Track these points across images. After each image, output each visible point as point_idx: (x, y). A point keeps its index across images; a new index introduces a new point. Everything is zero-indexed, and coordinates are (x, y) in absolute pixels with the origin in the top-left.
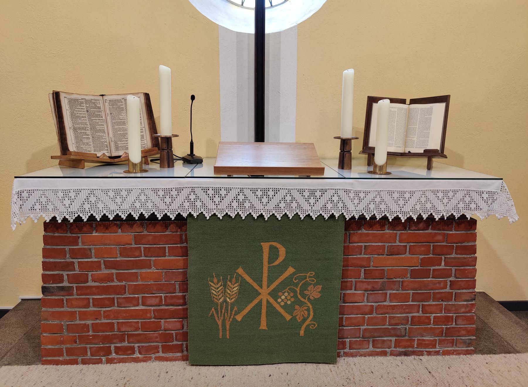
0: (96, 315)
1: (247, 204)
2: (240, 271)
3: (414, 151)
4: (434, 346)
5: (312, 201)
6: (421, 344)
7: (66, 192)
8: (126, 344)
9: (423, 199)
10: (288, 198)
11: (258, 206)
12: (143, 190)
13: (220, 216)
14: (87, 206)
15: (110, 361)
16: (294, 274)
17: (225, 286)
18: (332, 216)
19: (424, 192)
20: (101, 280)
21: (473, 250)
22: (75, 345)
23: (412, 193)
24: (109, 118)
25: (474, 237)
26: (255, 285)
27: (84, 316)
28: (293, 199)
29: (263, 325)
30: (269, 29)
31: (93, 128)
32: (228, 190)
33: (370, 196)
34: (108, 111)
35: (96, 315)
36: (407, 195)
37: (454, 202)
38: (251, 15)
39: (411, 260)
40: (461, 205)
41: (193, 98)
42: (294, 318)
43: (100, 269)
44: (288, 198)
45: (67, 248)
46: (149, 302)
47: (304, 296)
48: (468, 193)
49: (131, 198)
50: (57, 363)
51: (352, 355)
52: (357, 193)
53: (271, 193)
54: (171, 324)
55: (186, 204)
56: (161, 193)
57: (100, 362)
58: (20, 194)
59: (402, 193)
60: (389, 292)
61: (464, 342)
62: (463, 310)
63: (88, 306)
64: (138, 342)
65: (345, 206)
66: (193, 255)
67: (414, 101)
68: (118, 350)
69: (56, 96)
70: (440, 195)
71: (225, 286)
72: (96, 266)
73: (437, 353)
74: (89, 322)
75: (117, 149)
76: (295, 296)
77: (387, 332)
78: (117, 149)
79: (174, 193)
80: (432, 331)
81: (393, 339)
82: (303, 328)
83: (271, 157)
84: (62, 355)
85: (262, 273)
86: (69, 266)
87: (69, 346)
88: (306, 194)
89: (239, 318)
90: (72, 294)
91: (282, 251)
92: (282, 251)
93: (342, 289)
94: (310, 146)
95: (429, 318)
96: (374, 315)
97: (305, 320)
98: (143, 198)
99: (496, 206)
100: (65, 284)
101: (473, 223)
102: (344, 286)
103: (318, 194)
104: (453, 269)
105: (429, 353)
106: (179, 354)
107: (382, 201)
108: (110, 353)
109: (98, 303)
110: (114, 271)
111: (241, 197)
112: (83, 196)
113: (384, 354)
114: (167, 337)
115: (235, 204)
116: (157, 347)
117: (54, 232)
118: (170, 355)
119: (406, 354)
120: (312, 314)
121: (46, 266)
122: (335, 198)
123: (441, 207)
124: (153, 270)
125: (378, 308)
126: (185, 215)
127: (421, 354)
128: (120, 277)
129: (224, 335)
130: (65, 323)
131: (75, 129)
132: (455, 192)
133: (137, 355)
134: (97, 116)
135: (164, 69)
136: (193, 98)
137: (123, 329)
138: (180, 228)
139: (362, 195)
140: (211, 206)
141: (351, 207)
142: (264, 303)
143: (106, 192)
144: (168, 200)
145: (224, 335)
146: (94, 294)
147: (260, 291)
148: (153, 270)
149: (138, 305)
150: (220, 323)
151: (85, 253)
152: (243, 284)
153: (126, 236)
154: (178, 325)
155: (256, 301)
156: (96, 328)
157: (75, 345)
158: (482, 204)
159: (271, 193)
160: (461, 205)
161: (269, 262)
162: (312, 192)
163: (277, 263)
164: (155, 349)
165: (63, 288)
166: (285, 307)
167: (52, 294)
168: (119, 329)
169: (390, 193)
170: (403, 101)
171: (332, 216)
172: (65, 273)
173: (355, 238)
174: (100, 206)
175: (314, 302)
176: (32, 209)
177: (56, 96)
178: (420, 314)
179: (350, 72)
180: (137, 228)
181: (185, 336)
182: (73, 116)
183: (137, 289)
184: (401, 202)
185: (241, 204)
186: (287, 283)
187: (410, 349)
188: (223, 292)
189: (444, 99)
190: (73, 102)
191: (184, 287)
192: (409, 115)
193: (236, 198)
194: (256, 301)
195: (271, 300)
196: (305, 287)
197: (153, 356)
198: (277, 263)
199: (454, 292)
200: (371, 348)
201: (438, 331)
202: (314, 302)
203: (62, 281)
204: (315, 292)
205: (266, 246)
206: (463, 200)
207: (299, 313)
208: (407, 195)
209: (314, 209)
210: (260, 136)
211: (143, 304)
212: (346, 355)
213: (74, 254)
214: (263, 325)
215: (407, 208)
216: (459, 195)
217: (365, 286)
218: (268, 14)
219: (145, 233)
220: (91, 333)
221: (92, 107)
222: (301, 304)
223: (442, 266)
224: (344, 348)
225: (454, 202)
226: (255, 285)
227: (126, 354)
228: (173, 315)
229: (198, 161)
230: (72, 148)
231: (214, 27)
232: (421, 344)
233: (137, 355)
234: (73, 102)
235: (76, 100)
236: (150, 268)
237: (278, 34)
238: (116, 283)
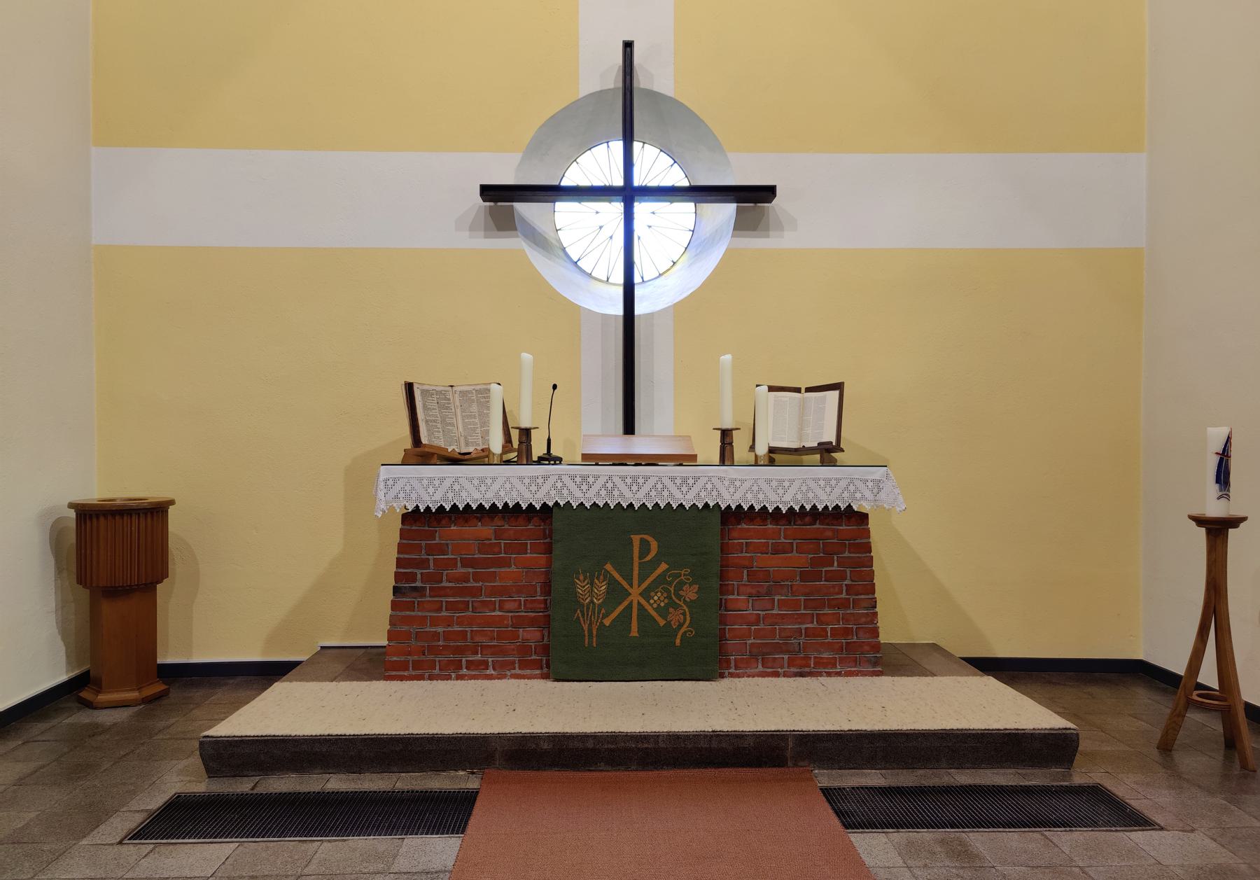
0: (449, 622)
1: (616, 493)
2: (608, 567)
3: (808, 445)
4: (834, 666)
5: (684, 489)
6: (819, 663)
7: (431, 480)
8: (479, 657)
9: (804, 488)
10: (659, 486)
11: (628, 494)
12: (508, 478)
13: (588, 505)
14: (450, 495)
15: (459, 677)
16: (667, 570)
17: (592, 584)
18: (706, 505)
19: (804, 481)
20: (457, 580)
21: (867, 548)
22: (423, 658)
23: (792, 481)
24: (458, 411)
25: (867, 533)
26: (624, 583)
27: (435, 621)
28: (664, 487)
29: (634, 632)
30: (639, 309)
31: (443, 421)
32: (597, 477)
33: (747, 485)
34: (458, 403)
35: (449, 622)
36: (786, 484)
37: (837, 491)
38: (619, 292)
39: (799, 559)
40: (846, 495)
41: (555, 387)
42: (668, 624)
43: (456, 567)
44: (659, 486)
45: (423, 543)
46: (507, 606)
47: (679, 597)
48: (852, 481)
49: (496, 487)
50: (401, 678)
51: (738, 676)
52: (732, 481)
53: (641, 481)
54: (530, 635)
55: (553, 492)
56: (527, 481)
57: (448, 678)
58: (386, 480)
59: (781, 481)
60: (776, 598)
61: (869, 661)
62: (863, 620)
63: (440, 609)
64: (493, 654)
65: (719, 494)
66: (558, 549)
67: (809, 390)
68: (470, 665)
69: (409, 387)
70: (822, 483)
71: (592, 584)
72: (452, 564)
73: (839, 674)
74: (440, 630)
75: (467, 444)
76: (669, 597)
77: (779, 648)
78: (467, 444)
79: (540, 481)
80: (829, 647)
81: (786, 657)
82: (679, 636)
83: (639, 445)
84: (407, 669)
85: (632, 569)
86: (423, 564)
87: (416, 658)
88: (678, 481)
89: (607, 622)
90: (425, 596)
91: (654, 545)
92: (654, 545)
93: (722, 593)
94: (687, 438)
95: (825, 630)
96: (762, 626)
97: (681, 625)
98: (508, 486)
99: (882, 495)
100: (418, 584)
101: (863, 517)
102: (723, 590)
103: (691, 481)
104: (848, 570)
105: (829, 674)
106: (538, 672)
107: (760, 490)
108: (461, 668)
109: (451, 607)
110: (471, 570)
111: (610, 485)
112: (447, 483)
113: (776, 675)
114: (524, 649)
115: (603, 492)
116: (514, 662)
117: (411, 525)
118: (528, 672)
119: (802, 675)
120: (688, 618)
121: (400, 563)
122: (709, 486)
123: (823, 497)
124: (513, 568)
125: (765, 617)
126: (551, 504)
127: (819, 674)
128: (477, 577)
129: (590, 643)
130: (414, 629)
131: (427, 421)
132: (838, 480)
133: (490, 671)
134: (447, 408)
135: (527, 357)
136: (555, 387)
137: (477, 639)
138: (544, 521)
139: (738, 483)
140: (578, 494)
141: (726, 496)
142: (635, 582)
143: (471, 480)
144: (534, 488)
145: (590, 643)
146: (446, 596)
147: (630, 591)
148: (513, 568)
149: (494, 610)
150: (586, 627)
151: (441, 549)
152: (612, 584)
153: (484, 530)
154: (538, 635)
155: (626, 603)
156: (447, 636)
157: (423, 658)
158: (868, 494)
159: (641, 481)
160: (846, 495)
161: (640, 558)
162: (685, 480)
163: (649, 558)
164: (511, 665)
165: (415, 589)
166: (658, 610)
167: (404, 595)
168: (472, 638)
169: (769, 481)
170: (798, 390)
171: (706, 505)
172: (419, 572)
173: (735, 534)
174: (464, 494)
175: (690, 604)
176: (396, 497)
177: (409, 387)
178: (815, 624)
179: (728, 357)
180: (498, 521)
181: (546, 649)
182: (425, 407)
183: (494, 591)
184: (781, 491)
185: (610, 493)
186: (661, 580)
187: (807, 670)
188: (591, 592)
189: (838, 387)
190: (424, 392)
191: (547, 588)
192: (803, 407)
193: (604, 486)
194: (626, 603)
195: (643, 602)
196: (680, 586)
197: (508, 673)
198: (649, 558)
199: (852, 598)
200: (760, 668)
201: (837, 646)
202: (690, 604)
203: (415, 580)
204: (691, 593)
205: (636, 539)
206: (847, 488)
207: (675, 617)
208: (786, 484)
209: (688, 499)
210: (629, 428)
211: (500, 610)
212: (732, 675)
213: (430, 550)
214: (634, 632)
215: (787, 498)
216: (843, 484)
217: (749, 590)
218: (638, 292)
219: (507, 527)
220: (441, 643)
221: (442, 398)
222: (676, 607)
223: (835, 567)
224: (728, 667)
225: (837, 491)
226: (624, 583)
227: (478, 670)
228: (533, 622)
229: (558, 460)
230: (424, 440)
231: (575, 309)
232: (819, 663)
233: (490, 671)
234: (424, 392)
235: (427, 391)
236: (510, 566)
237: (651, 316)
238: (472, 584)
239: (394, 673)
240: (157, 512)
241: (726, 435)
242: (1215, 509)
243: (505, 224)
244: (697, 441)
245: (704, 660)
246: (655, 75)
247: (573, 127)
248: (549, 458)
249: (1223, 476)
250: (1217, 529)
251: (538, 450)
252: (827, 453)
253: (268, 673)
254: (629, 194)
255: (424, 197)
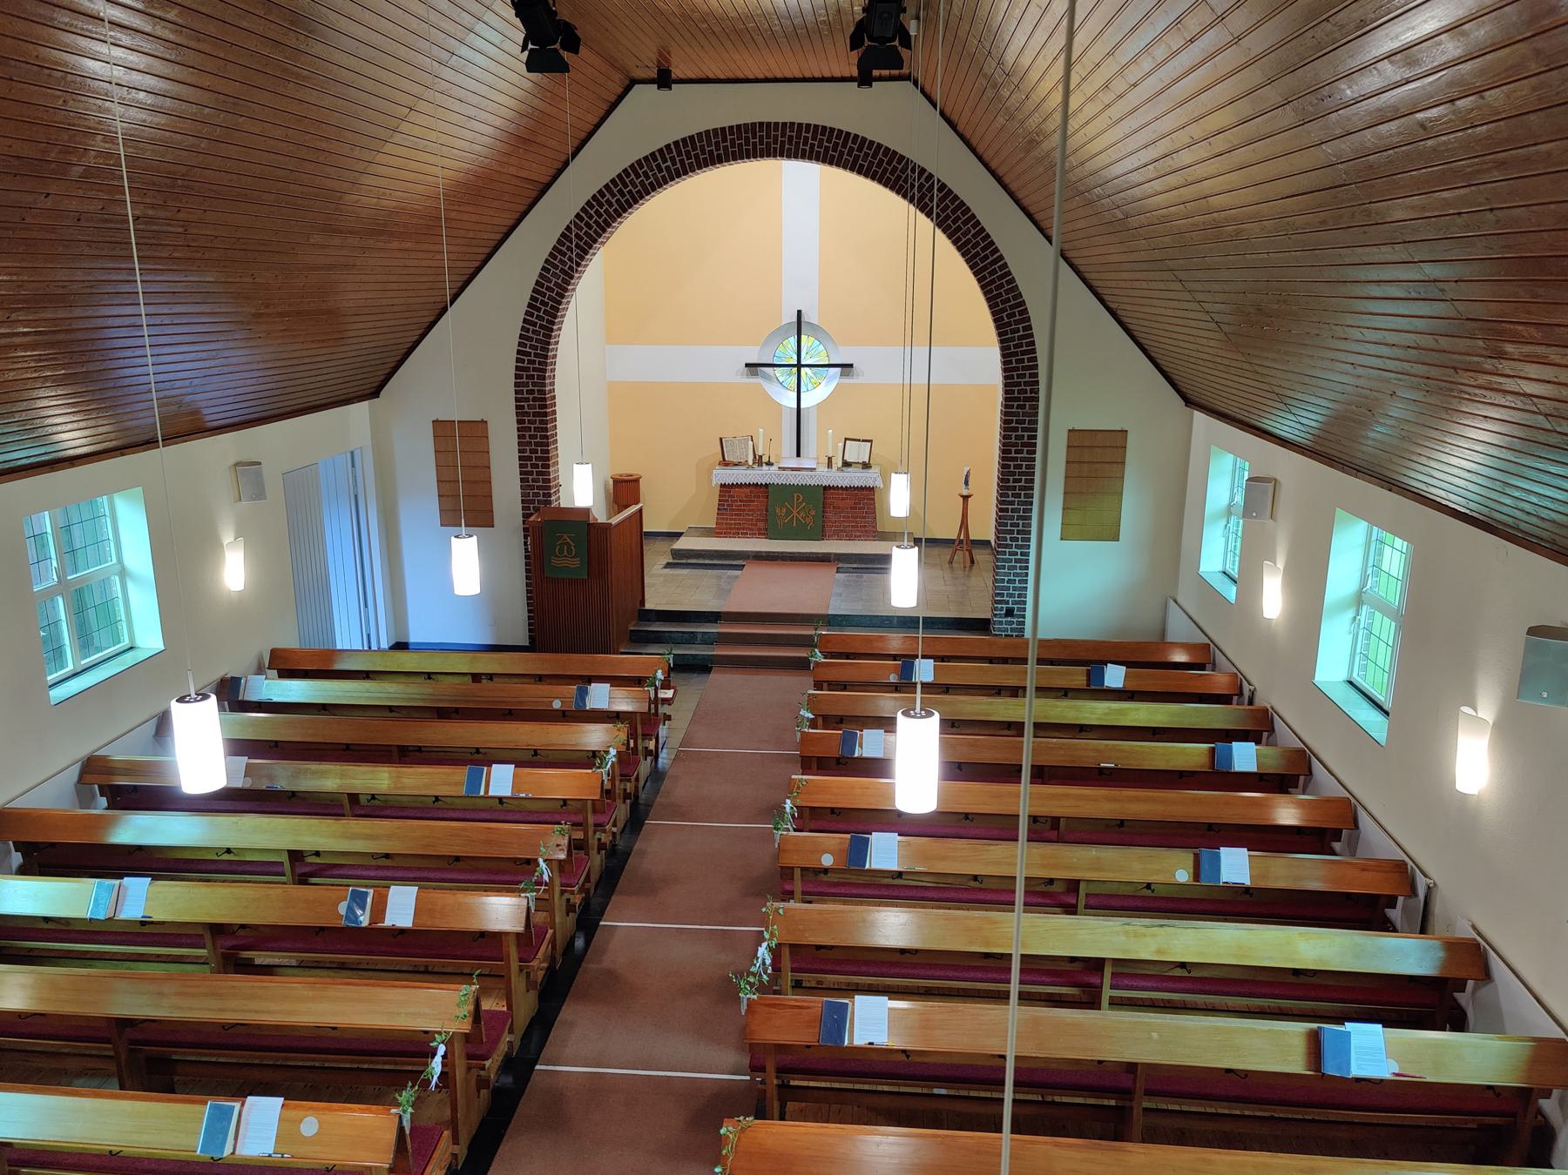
30: (803, 406)
54: (761, 525)
182: (1067, 796)
239: (1431, 79)
240: (637, 481)
241: (830, 459)
242: (965, 493)
243: (755, 374)
244: (815, 466)
245: (822, 535)
246: (810, 317)
247: (779, 334)
248: (769, 464)
249: (966, 483)
250: (966, 498)
251: (765, 459)
252: (866, 466)
253: (679, 535)
254: (799, 366)
255: (722, 364)
